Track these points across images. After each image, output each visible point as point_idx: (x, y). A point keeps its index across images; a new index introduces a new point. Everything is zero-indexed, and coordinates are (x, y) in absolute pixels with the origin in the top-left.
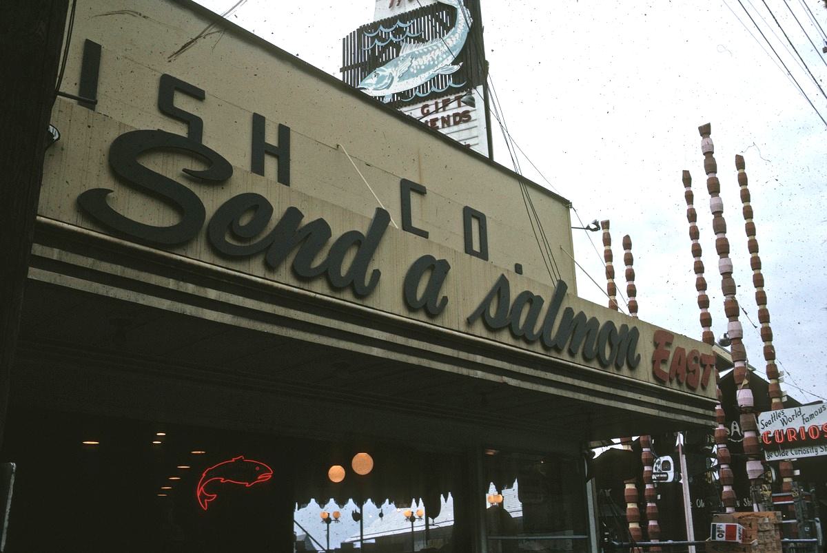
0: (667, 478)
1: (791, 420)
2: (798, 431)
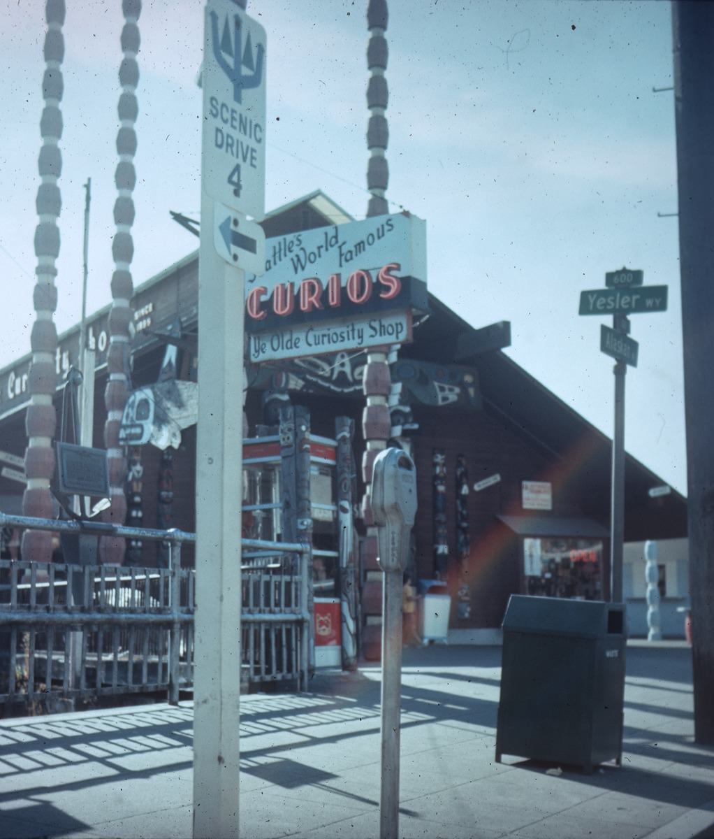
0: (140, 436)
1: (312, 258)
2: (324, 287)
